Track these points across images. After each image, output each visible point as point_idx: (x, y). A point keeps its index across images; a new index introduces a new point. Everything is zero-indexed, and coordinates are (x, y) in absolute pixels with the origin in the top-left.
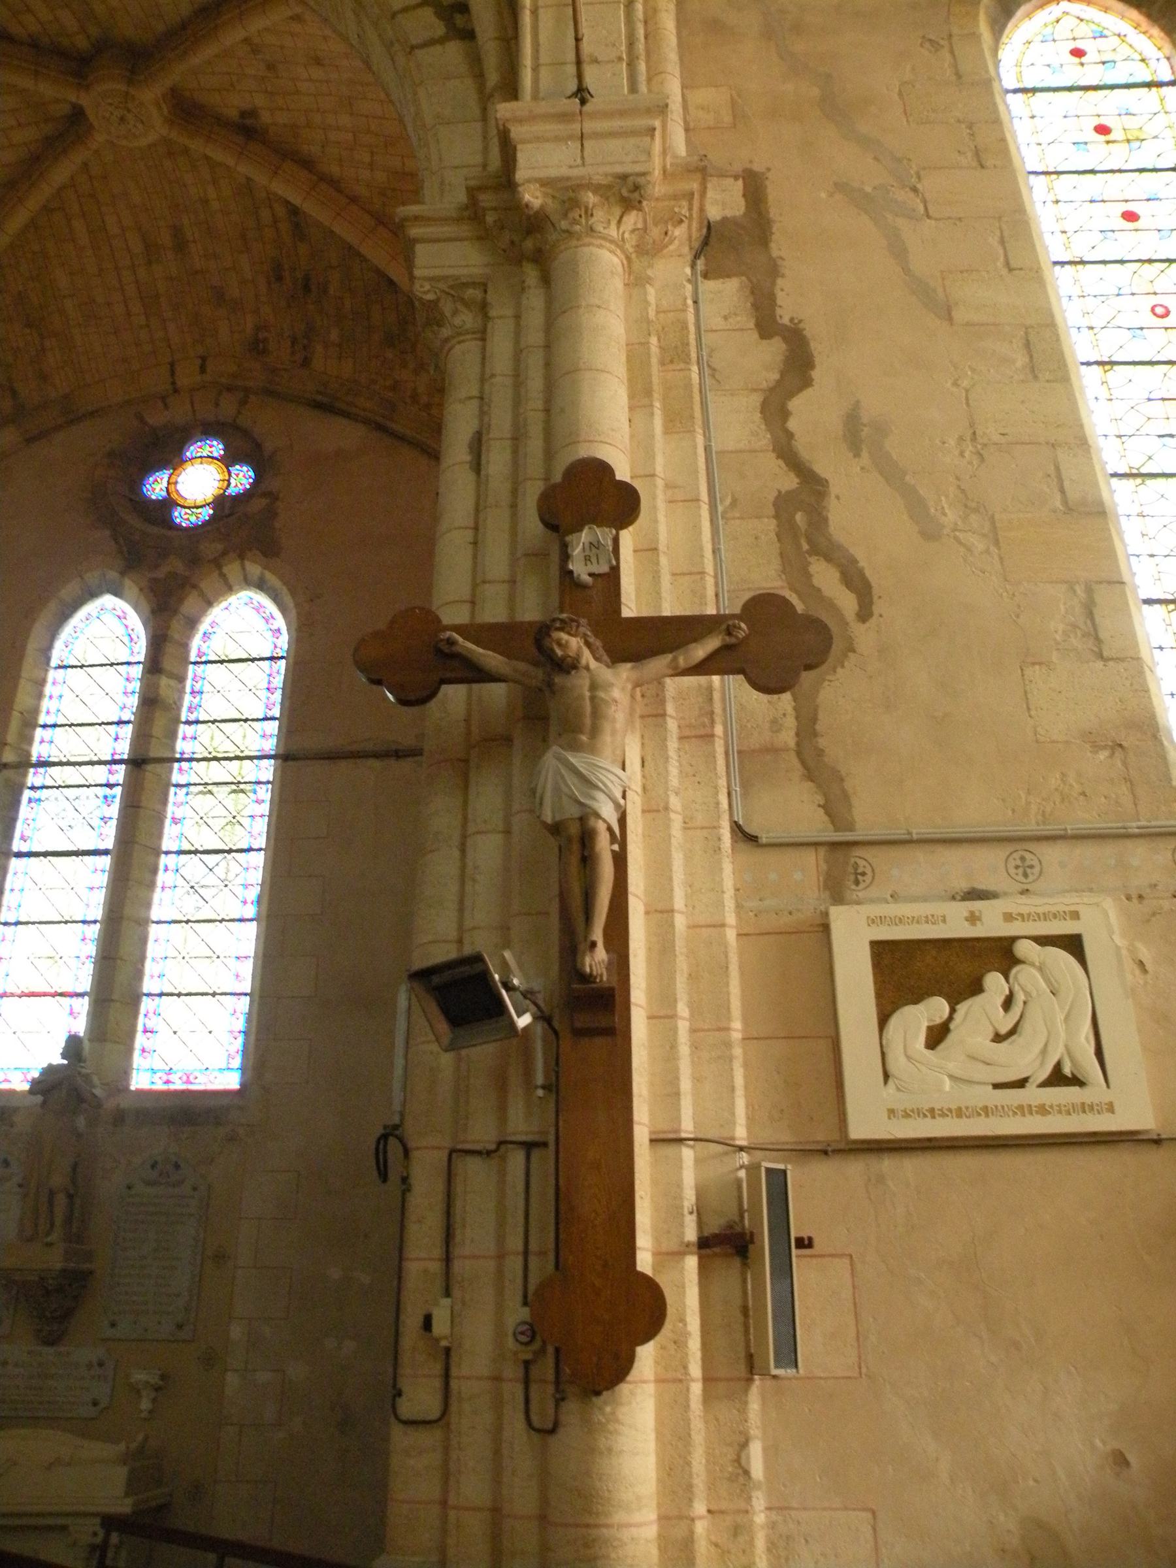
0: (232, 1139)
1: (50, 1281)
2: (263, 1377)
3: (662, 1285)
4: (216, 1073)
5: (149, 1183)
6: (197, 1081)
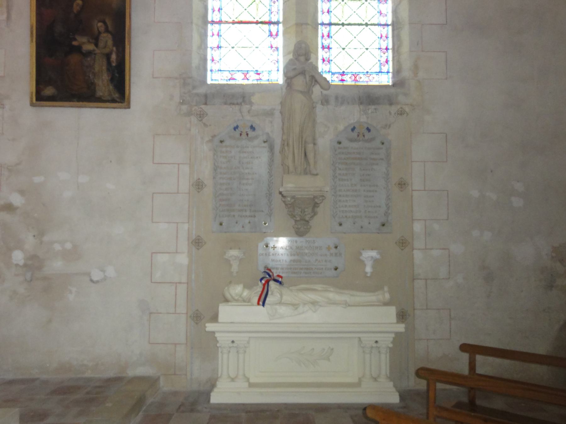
0: (401, 113)
1: (289, 199)
2: (436, 253)
3: (421, 366)
4: (374, 75)
5: (351, 140)
6: (361, 80)
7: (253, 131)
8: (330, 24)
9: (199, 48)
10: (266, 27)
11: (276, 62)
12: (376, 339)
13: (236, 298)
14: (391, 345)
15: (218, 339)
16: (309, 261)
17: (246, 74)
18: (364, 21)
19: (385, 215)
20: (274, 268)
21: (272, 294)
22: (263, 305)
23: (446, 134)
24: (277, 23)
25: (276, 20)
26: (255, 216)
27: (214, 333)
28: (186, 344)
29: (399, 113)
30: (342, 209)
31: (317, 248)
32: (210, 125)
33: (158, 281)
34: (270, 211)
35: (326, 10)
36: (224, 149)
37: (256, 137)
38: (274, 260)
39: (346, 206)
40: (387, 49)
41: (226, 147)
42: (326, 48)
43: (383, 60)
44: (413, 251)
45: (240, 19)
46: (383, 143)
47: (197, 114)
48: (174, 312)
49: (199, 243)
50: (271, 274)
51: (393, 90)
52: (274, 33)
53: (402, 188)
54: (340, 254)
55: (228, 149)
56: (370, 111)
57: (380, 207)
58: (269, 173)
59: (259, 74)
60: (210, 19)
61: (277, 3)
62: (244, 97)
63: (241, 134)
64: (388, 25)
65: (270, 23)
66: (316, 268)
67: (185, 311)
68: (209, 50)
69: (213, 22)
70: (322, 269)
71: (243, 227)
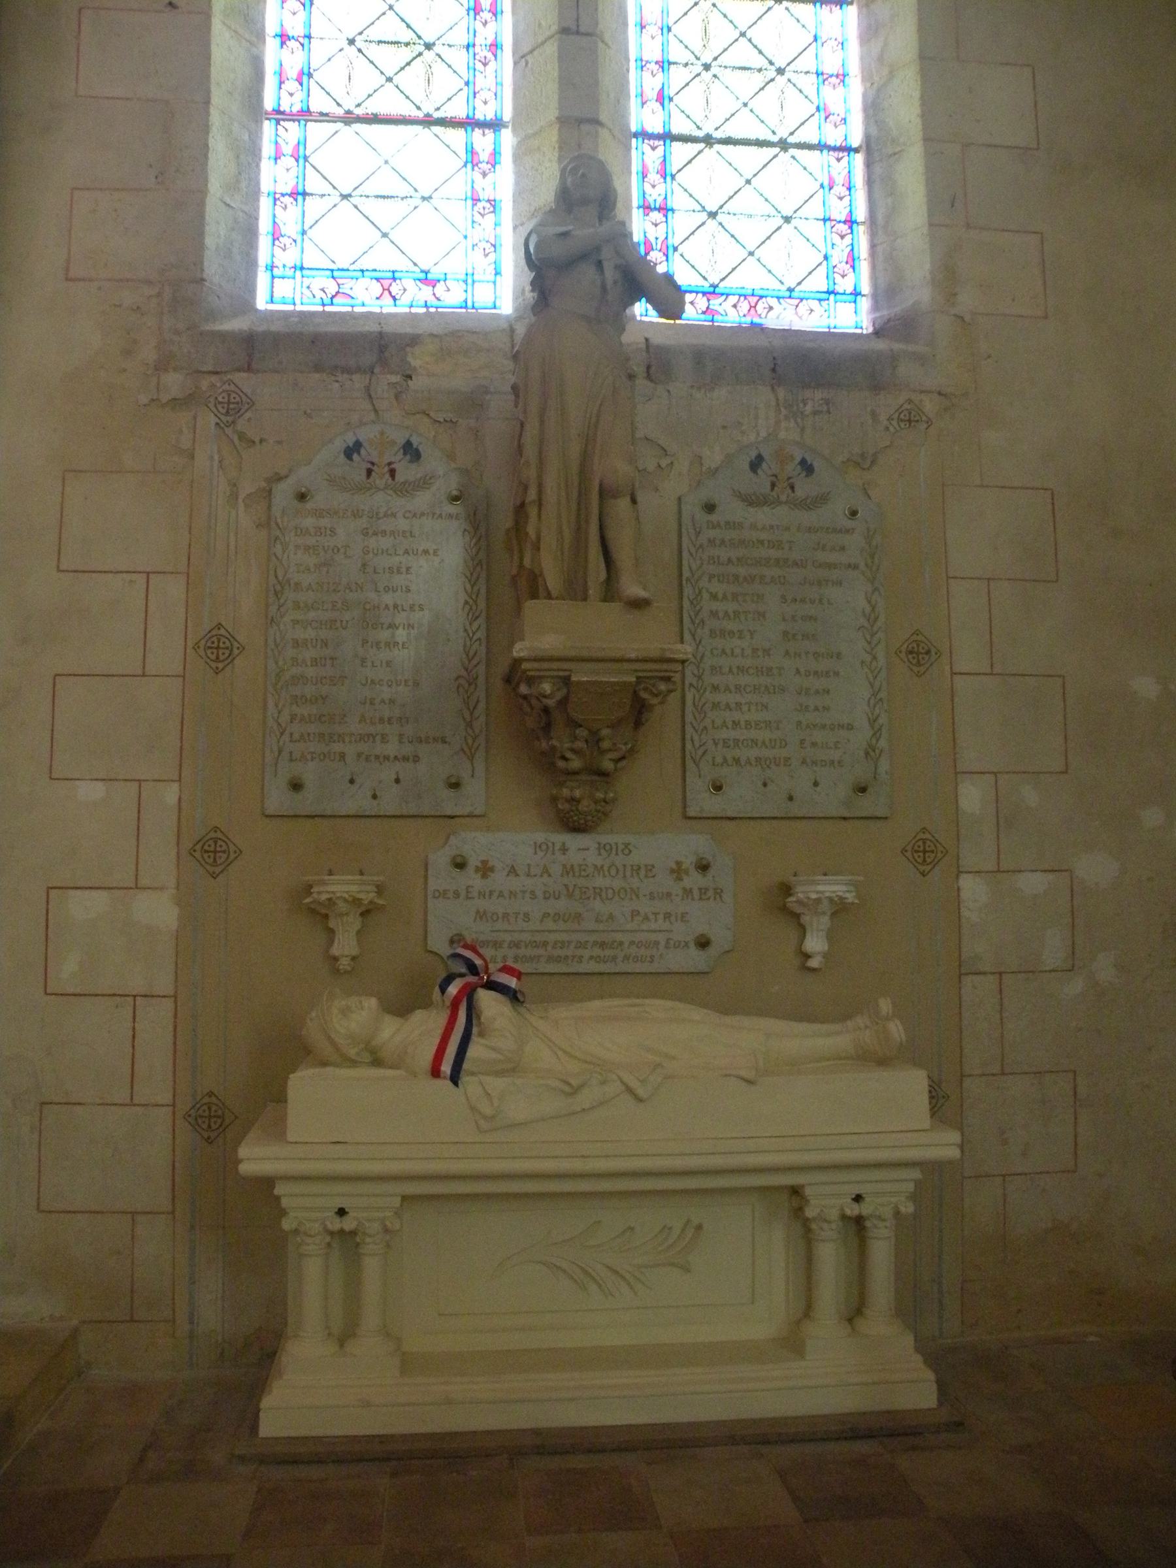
0: (910, 418)
2: (1033, 883)
5: (752, 501)
7: (411, 461)
8: (668, 137)
9: (232, 186)
10: (456, 137)
11: (489, 245)
12: (856, 1190)
13: (352, 1052)
14: (908, 1208)
15: (284, 1202)
16: (611, 917)
17: (388, 281)
18: (774, 133)
19: (867, 754)
20: (485, 943)
21: (481, 1034)
22: (455, 1079)
23: (1052, 494)
24: (494, 125)
25: (490, 116)
26: (416, 759)
27: (268, 1182)
28: (173, 1212)
29: (902, 416)
30: (724, 734)
31: (637, 869)
32: (261, 441)
33: (71, 990)
34: (470, 741)
35: (652, 94)
36: (309, 522)
37: (424, 483)
38: (485, 912)
39: (736, 724)
40: (850, 222)
41: (319, 513)
42: (655, 209)
43: (839, 255)
44: (957, 877)
45: (371, 107)
46: (854, 513)
47: (217, 403)
48: (128, 1101)
49: (215, 852)
50: (478, 962)
51: (881, 345)
52: (484, 156)
53: (919, 664)
54: (718, 893)
55: (325, 522)
56: (808, 409)
57: (850, 727)
58: (468, 607)
59: (433, 283)
60: (269, 104)
61: (492, 66)
62: (382, 349)
63: (369, 472)
64: (848, 150)
65: (469, 123)
66: (632, 943)
67: (166, 1098)
68: (265, 204)
69: (280, 115)
70: (657, 943)
71: (375, 797)
